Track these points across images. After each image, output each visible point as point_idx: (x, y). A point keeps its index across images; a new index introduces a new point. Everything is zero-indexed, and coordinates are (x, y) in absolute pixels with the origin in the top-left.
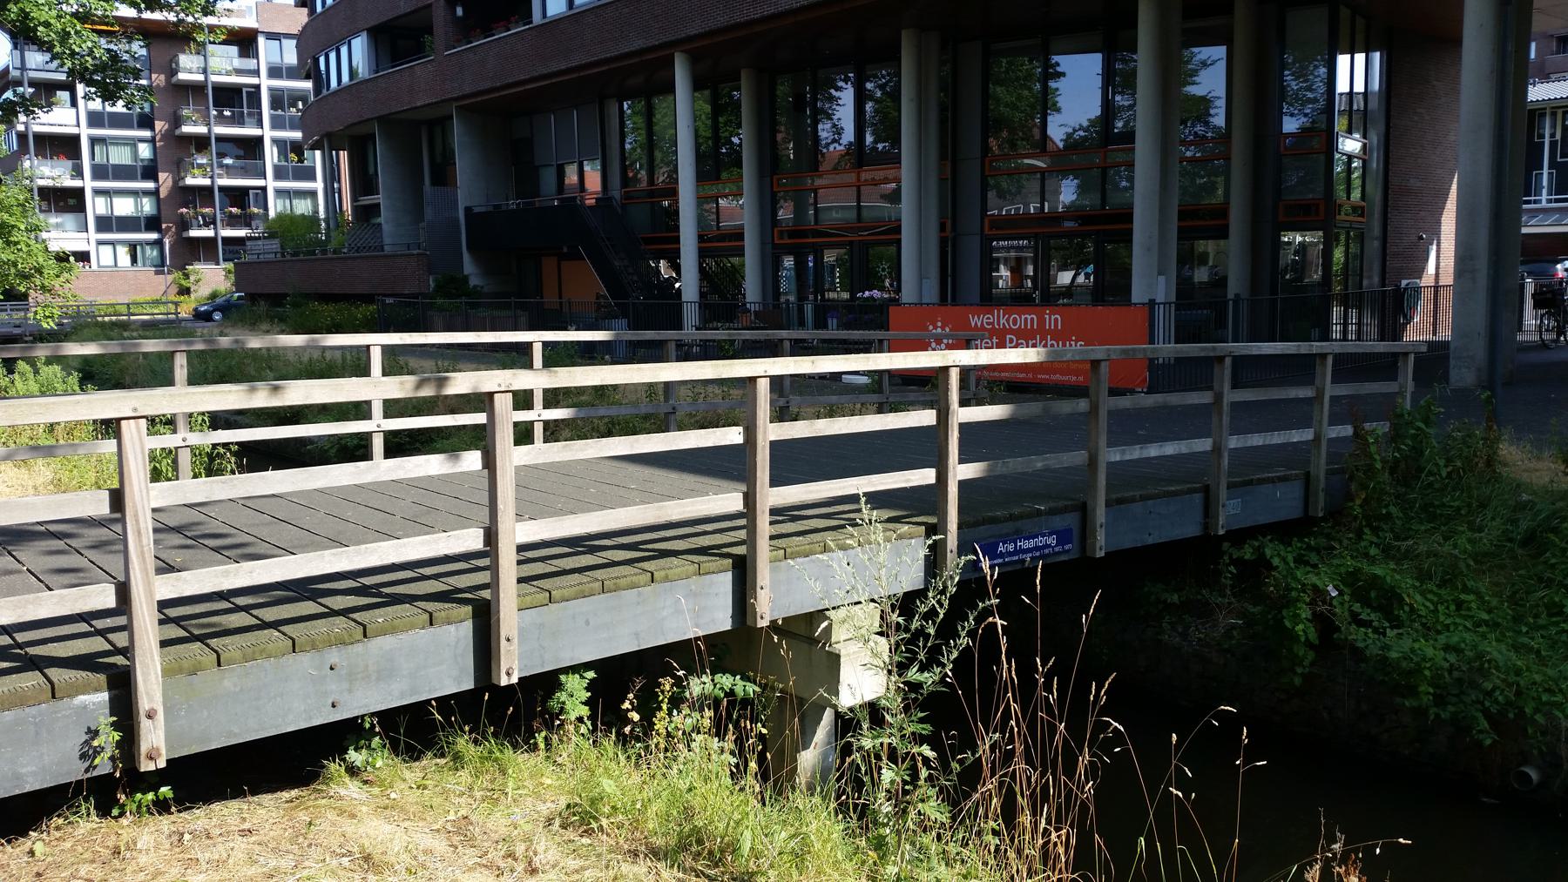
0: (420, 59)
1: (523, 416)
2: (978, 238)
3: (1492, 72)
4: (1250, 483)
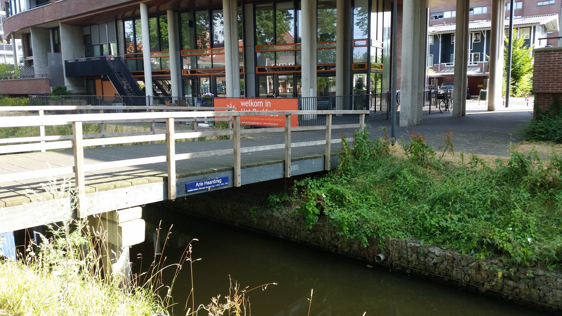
0: (48, 3)
2: (254, 75)
3: (412, 18)
4: (302, 159)
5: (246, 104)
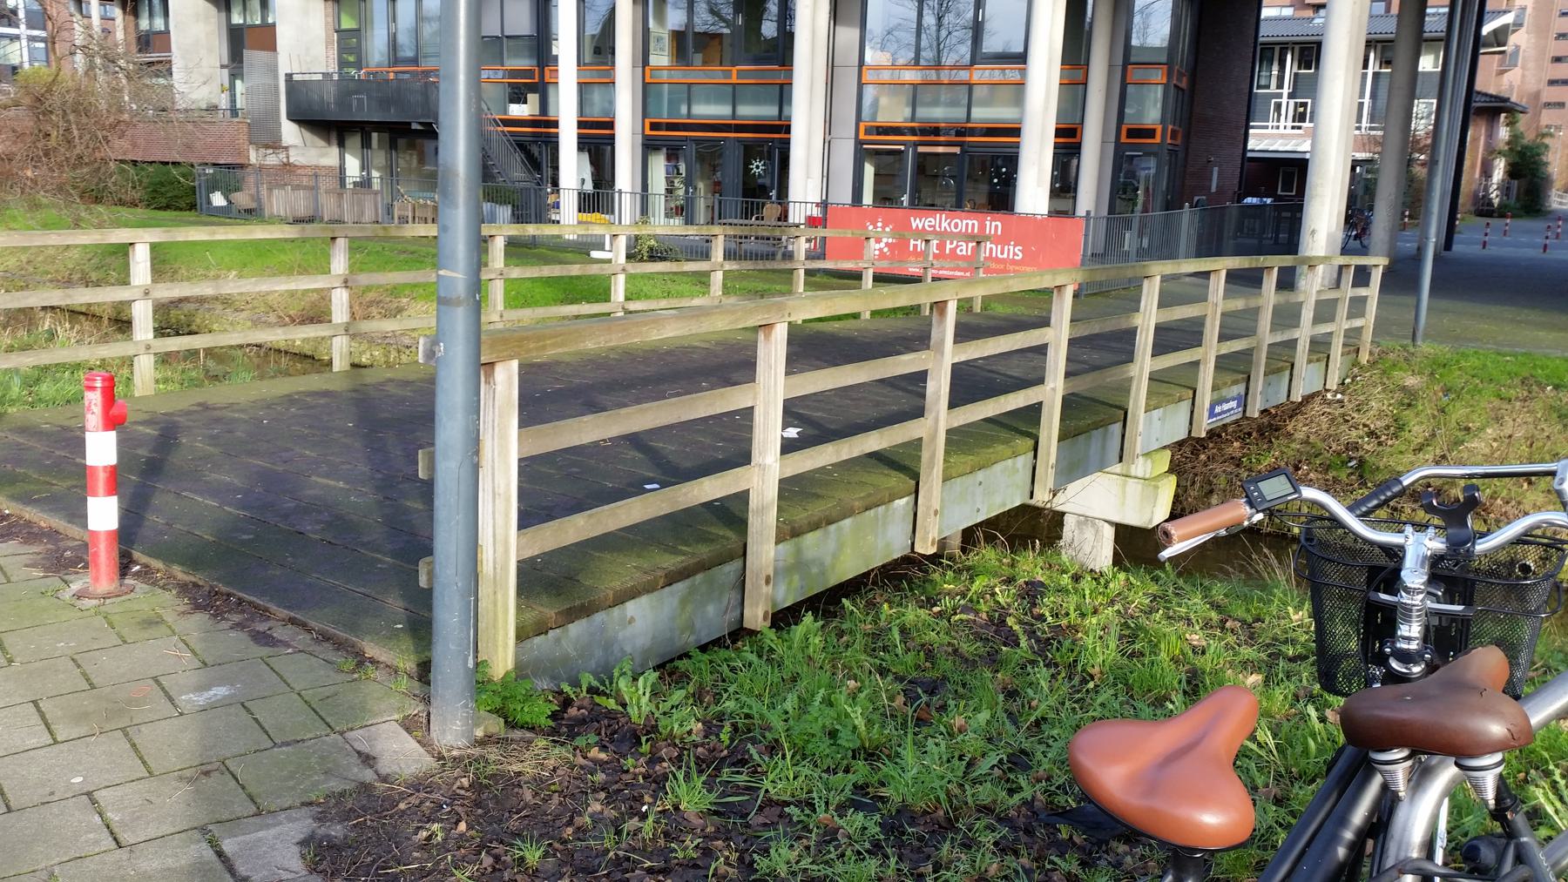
5: (927, 224)
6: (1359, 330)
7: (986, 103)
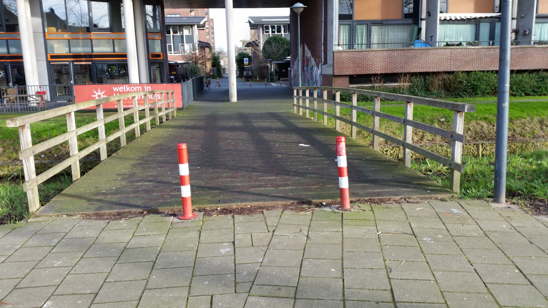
1: (21, 103)
6: (145, 124)
7: (98, 46)
